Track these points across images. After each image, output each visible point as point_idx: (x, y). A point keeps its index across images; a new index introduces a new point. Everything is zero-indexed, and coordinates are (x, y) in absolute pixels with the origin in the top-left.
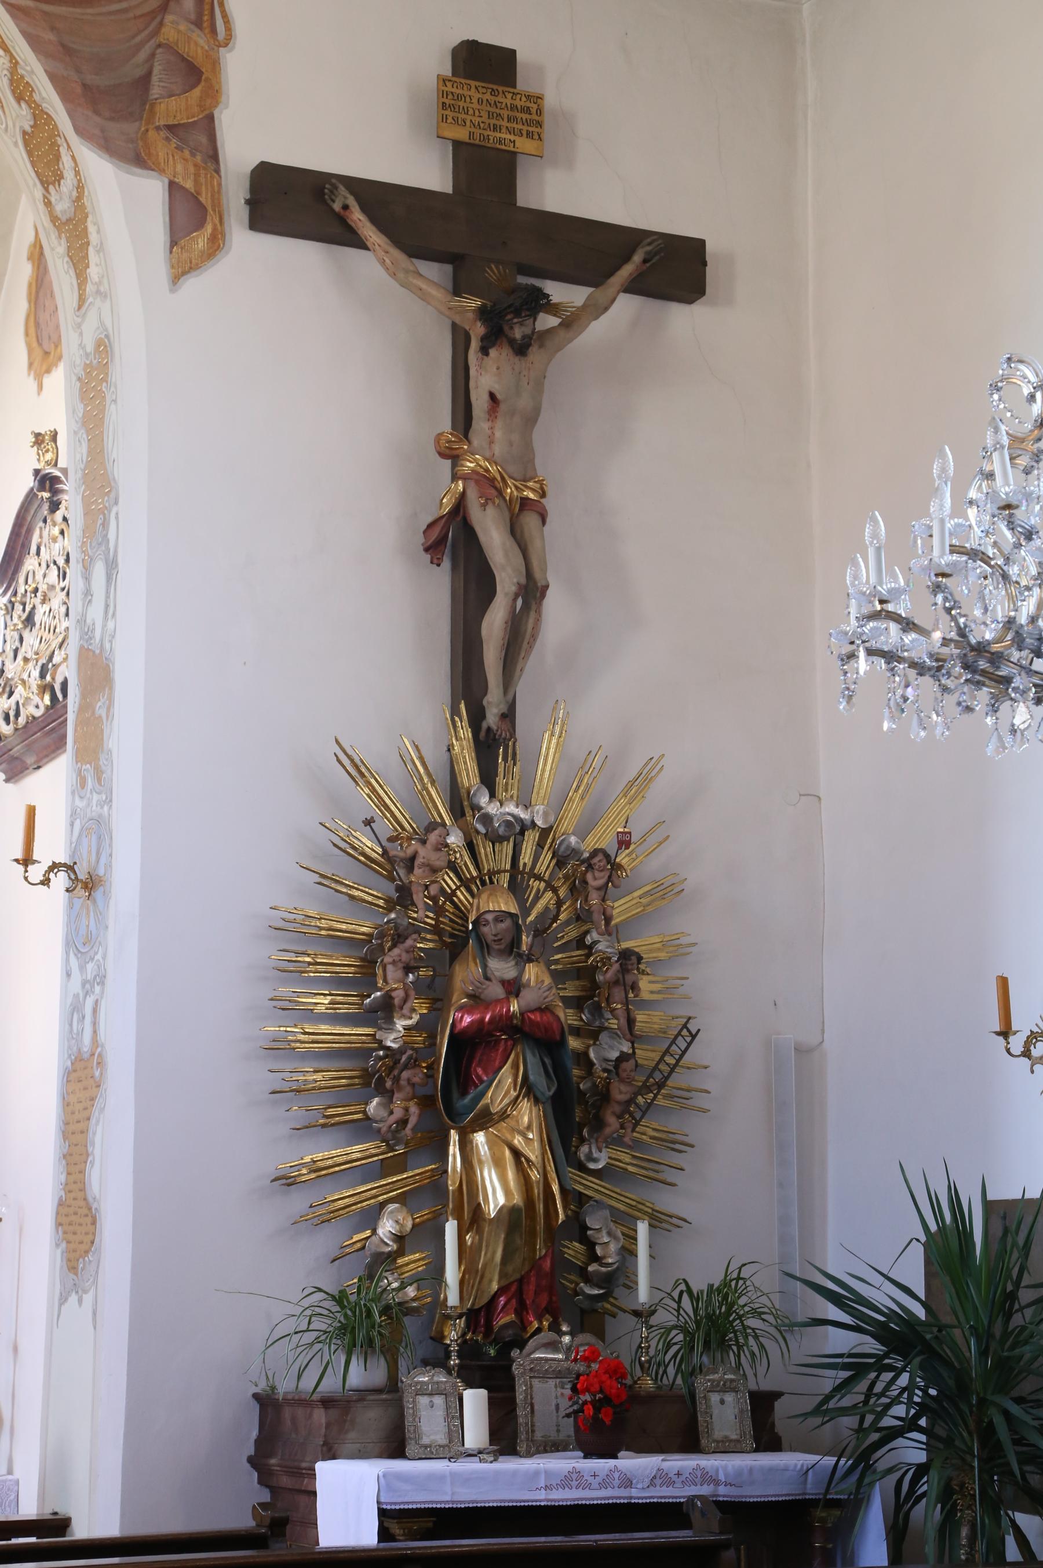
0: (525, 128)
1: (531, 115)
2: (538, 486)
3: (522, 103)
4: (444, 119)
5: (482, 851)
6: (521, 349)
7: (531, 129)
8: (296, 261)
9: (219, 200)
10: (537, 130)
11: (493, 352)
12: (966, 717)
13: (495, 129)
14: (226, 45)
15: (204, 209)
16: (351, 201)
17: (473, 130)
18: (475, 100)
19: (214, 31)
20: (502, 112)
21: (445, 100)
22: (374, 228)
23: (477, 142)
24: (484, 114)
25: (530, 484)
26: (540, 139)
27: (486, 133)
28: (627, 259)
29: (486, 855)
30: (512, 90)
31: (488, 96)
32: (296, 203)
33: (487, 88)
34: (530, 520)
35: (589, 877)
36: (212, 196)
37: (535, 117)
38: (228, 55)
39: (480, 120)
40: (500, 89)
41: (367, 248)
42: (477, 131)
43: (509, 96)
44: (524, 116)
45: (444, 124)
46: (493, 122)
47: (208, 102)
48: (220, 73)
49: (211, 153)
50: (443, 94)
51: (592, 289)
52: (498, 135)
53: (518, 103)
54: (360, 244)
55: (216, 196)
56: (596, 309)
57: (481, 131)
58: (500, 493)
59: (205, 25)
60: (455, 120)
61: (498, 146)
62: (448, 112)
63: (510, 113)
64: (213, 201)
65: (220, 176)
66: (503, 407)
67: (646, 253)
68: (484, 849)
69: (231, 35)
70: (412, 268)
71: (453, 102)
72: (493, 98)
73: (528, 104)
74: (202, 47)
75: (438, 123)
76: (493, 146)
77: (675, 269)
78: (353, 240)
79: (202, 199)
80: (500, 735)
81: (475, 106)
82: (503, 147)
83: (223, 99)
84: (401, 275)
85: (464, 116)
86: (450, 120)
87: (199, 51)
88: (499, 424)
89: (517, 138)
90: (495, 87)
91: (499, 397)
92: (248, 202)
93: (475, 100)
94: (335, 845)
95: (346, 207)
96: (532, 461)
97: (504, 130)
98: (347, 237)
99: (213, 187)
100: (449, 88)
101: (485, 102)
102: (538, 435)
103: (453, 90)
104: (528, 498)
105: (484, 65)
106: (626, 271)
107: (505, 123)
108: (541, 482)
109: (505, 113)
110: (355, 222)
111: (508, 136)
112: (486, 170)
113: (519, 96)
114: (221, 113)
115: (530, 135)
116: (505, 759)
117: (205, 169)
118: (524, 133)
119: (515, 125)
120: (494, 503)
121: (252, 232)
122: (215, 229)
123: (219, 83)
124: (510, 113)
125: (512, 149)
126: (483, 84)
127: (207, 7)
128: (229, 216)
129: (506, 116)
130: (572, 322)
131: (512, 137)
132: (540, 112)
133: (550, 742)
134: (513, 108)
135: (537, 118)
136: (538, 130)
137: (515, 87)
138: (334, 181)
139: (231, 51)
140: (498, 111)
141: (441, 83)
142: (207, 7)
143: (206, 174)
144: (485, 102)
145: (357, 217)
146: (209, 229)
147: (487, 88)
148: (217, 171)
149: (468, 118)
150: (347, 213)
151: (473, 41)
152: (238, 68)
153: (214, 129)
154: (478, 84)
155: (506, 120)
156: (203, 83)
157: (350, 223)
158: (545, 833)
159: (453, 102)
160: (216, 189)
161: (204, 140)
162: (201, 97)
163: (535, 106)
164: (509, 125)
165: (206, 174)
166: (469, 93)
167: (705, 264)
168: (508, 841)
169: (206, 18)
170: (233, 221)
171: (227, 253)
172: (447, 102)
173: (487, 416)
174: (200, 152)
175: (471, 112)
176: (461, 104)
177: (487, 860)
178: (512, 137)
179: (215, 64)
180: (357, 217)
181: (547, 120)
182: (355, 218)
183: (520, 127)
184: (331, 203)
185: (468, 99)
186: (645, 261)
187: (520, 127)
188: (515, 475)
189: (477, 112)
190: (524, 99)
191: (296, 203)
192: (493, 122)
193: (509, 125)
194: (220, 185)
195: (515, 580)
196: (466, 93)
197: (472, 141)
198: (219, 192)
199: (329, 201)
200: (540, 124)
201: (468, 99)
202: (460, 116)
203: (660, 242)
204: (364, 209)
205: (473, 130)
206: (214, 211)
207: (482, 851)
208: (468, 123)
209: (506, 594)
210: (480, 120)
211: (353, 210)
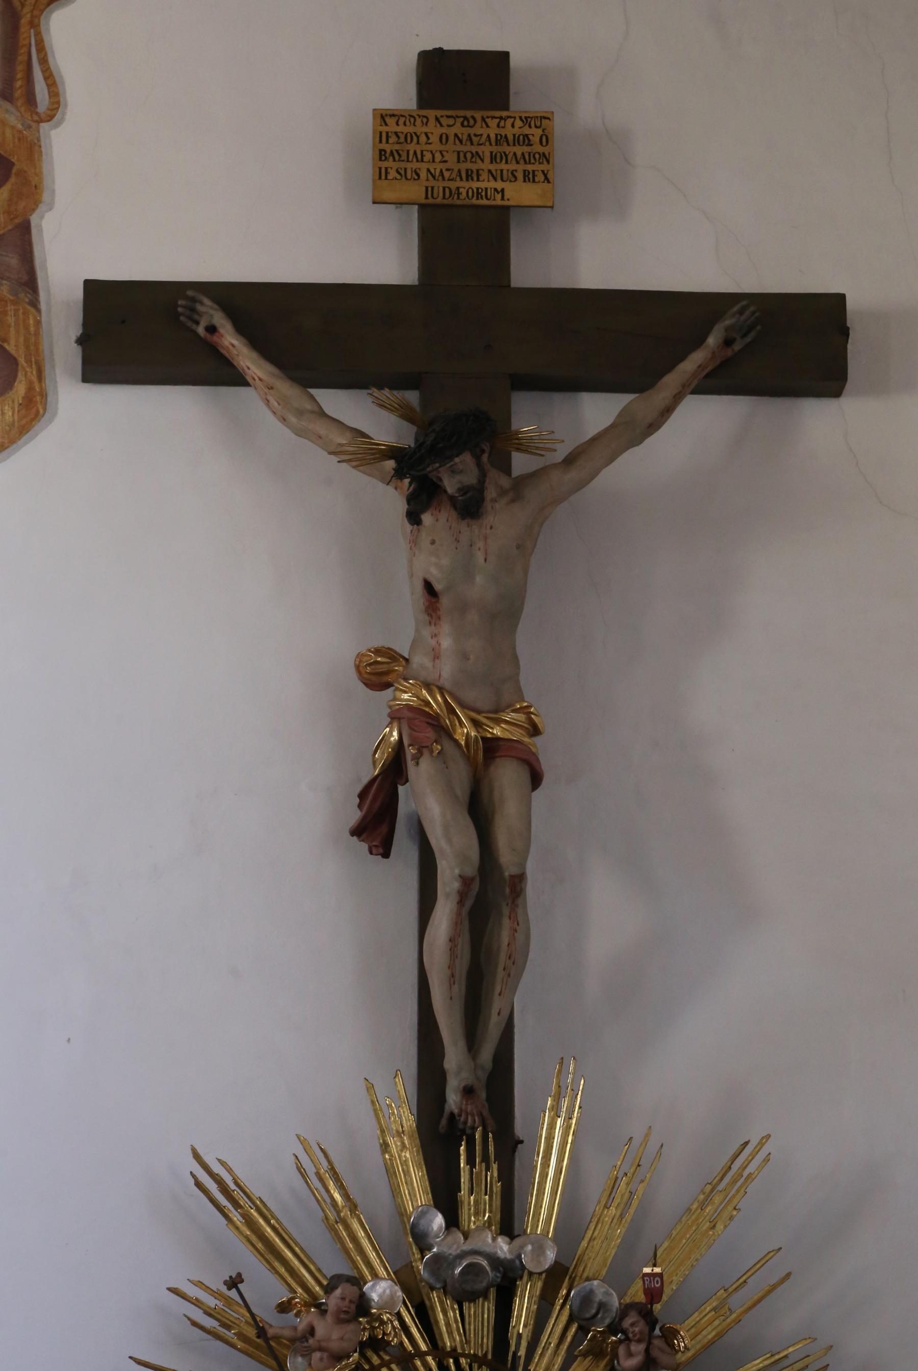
0: (521, 167)
1: (534, 148)
2: (521, 717)
3: (516, 131)
4: (381, 174)
5: (441, 1316)
6: (470, 507)
7: (530, 168)
8: (161, 417)
9: (37, 345)
10: (542, 167)
11: (427, 518)
12: (71, 1041)
13: (469, 176)
14: (50, 118)
15: (14, 361)
16: (219, 319)
17: (432, 183)
18: (434, 139)
19: (31, 100)
20: (480, 149)
21: (384, 146)
22: (254, 355)
23: (439, 200)
24: (451, 158)
25: (509, 716)
26: (547, 179)
27: (453, 185)
28: (699, 342)
29: (448, 1325)
30: (504, 114)
31: (457, 129)
32: (147, 333)
33: (455, 118)
34: (507, 777)
35: (621, 1350)
36: (26, 340)
37: (538, 148)
38: (53, 133)
39: (443, 166)
40: (478, 115)
41: (246, 384)
42: (439, 185)
43: (493, 123)
44: (519, 150)
45: (385, 183)
46: (464, 166)
47: (22, 204)
48: (40, 160)
49: (25, 278)
50: (380, 137)
51: (632, 396)
52: (475, 185)
53: (509, 132)
54: (238, 379)
55: (33, 339)
56: (631, 432)
57: (446, 184)
58: (445, 733)
59: (18, 93)
60: (402, 174)
61: (474, 201)
62: (390, 163)
63: (495, 149)
64: (27, 347)
65: (39, 311)
66: (445, 602)
67: (727, 329)
68: (445, 1314)
69: (58, 103)
70: (308, 406)
71: (397, 147)
72: (467, 131)
73: (526, 130)
74: (13, 127)
75: (374, 181)
76: (467, 202)
77: (790, 346)
78: (227, 375)
79: (10, 348)
80: (465, 1123)
81: (436, 146)
82: (484, 202)
83: (46, 197)
84: (293, 419)
85: (415, 165)
86: (392, 174)
87: (8, 133)
88: (445, 628)
89: (507, 186)
90: (469, 114)
91: (438, 587)
92: (80, 341)
93: (434, 139)
94: (194, 1324)
95: (212, 329)
96: (514, 678)
97: (484, 175)
98: (222, 374)
99: (27, 328)
100: (392, 127)
101: (451, 138)
102: (526, 640)
103: (398, 129)
104: (497, 739)
105: (463, 82)
106: (693, 363)
107: (486, 165)
108: (525, 710)
109: (486, 150)
110: (227, 349)
111: (492, 184)
112: (464, 238)
113: (510, 121)
114: (42, 217)
115: (529, 177)
116: (471, 1161)
117: (13, 303)
118: (520, 176)
119: (503, 166)
120: (432, 752)
121: (86, 385)
122: (30, 389)
123: (39, 175)
124: (495, 149)
125: (499, 202)
126: (449, 113)
127: (20, 68)
128: (53, 367)
129: (487, 154)
130: (587, 457)
131: (499, 185)
132: (546, 139)
133: (552, 1126)
134: (500, 140)
135: (540, 149)
136: (544, 167)
137: (507, 108)
138: (190, 293)
139: (57, 125)
140: (474, 149)
141: (379, 120)
142: (20, 68)
143: (16, 311)
144: (451, 138)
145: (231, 341)
146: (20, 388)
147: (455, 118)
148: (35, 303)
149: (424, 167)
150: (215, 338)
151: (435, 49)
152: (66, 151)
153: (30, 243)
154: (439, 113)
155: (487, 159)
156: (13, 179)
157: (222, 351)
158: (556, 1275)
159: (397, 147)
160: (32, 329)
161: (13, 261)
162: (10, 200)
163: (539, 132)
164: (492, 167)
165: (16, 311)
166: (425, 129)
167: (845, 332)
168: (486, 1297)
169: (19, 84)
170: (58, 371)
171: (51, 421)
172: (388, 148)
173: (427, 618)
174: (8, 279)
175: (428, 156)
176: (412, 147)
177: (450, 1333)
178: (499, 185)
179: (33, 149)
180: (231, 341)
181: (561, 150)
182: (226, 343)
183: (512, 166)
184: (194, 327)
185: (423, 139)
186: (728, 343)
187: (512, 166)
188: (479, 705)
189: (438, 157)
190: (518, 123)
191: (147, 333)
192: (464, 166)
193: (492, 167)
194: (38, 323)
195: (457, 871)
196: (420, 129)
197: (431, 201)
198: (37, 334)
199: (189, 324)
200: (546, 158)
201: (423, 139)
202: (409, 166)
203: (752, 309)
204: (241, 329)
205: (432, 183)
206: (29, 361)
207: (441, 1316)
208: (423, 174)
209: (447, 895)
210: (443, 166)
211: (221, 331)
